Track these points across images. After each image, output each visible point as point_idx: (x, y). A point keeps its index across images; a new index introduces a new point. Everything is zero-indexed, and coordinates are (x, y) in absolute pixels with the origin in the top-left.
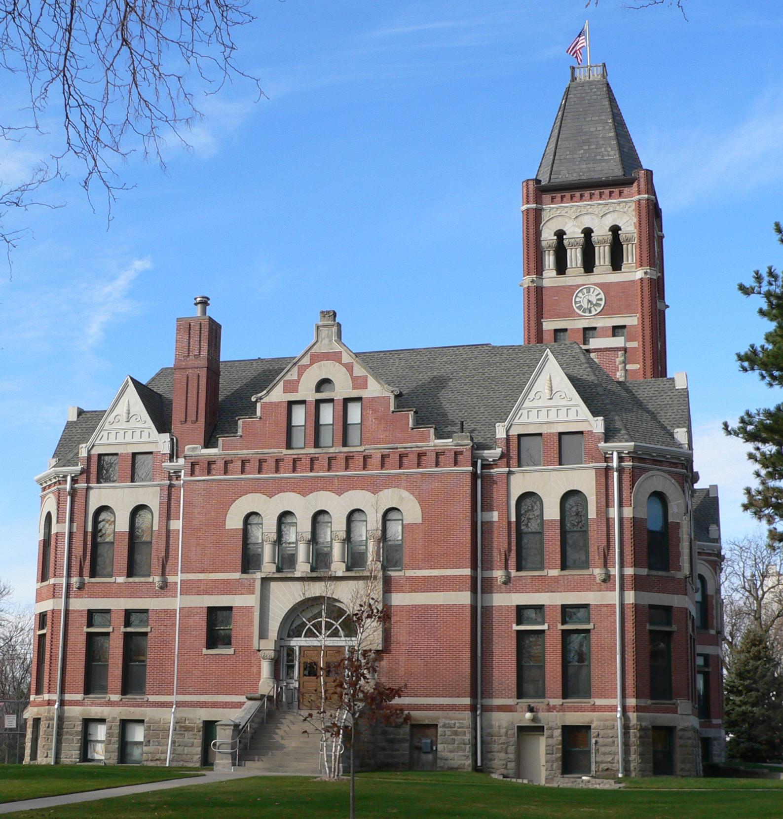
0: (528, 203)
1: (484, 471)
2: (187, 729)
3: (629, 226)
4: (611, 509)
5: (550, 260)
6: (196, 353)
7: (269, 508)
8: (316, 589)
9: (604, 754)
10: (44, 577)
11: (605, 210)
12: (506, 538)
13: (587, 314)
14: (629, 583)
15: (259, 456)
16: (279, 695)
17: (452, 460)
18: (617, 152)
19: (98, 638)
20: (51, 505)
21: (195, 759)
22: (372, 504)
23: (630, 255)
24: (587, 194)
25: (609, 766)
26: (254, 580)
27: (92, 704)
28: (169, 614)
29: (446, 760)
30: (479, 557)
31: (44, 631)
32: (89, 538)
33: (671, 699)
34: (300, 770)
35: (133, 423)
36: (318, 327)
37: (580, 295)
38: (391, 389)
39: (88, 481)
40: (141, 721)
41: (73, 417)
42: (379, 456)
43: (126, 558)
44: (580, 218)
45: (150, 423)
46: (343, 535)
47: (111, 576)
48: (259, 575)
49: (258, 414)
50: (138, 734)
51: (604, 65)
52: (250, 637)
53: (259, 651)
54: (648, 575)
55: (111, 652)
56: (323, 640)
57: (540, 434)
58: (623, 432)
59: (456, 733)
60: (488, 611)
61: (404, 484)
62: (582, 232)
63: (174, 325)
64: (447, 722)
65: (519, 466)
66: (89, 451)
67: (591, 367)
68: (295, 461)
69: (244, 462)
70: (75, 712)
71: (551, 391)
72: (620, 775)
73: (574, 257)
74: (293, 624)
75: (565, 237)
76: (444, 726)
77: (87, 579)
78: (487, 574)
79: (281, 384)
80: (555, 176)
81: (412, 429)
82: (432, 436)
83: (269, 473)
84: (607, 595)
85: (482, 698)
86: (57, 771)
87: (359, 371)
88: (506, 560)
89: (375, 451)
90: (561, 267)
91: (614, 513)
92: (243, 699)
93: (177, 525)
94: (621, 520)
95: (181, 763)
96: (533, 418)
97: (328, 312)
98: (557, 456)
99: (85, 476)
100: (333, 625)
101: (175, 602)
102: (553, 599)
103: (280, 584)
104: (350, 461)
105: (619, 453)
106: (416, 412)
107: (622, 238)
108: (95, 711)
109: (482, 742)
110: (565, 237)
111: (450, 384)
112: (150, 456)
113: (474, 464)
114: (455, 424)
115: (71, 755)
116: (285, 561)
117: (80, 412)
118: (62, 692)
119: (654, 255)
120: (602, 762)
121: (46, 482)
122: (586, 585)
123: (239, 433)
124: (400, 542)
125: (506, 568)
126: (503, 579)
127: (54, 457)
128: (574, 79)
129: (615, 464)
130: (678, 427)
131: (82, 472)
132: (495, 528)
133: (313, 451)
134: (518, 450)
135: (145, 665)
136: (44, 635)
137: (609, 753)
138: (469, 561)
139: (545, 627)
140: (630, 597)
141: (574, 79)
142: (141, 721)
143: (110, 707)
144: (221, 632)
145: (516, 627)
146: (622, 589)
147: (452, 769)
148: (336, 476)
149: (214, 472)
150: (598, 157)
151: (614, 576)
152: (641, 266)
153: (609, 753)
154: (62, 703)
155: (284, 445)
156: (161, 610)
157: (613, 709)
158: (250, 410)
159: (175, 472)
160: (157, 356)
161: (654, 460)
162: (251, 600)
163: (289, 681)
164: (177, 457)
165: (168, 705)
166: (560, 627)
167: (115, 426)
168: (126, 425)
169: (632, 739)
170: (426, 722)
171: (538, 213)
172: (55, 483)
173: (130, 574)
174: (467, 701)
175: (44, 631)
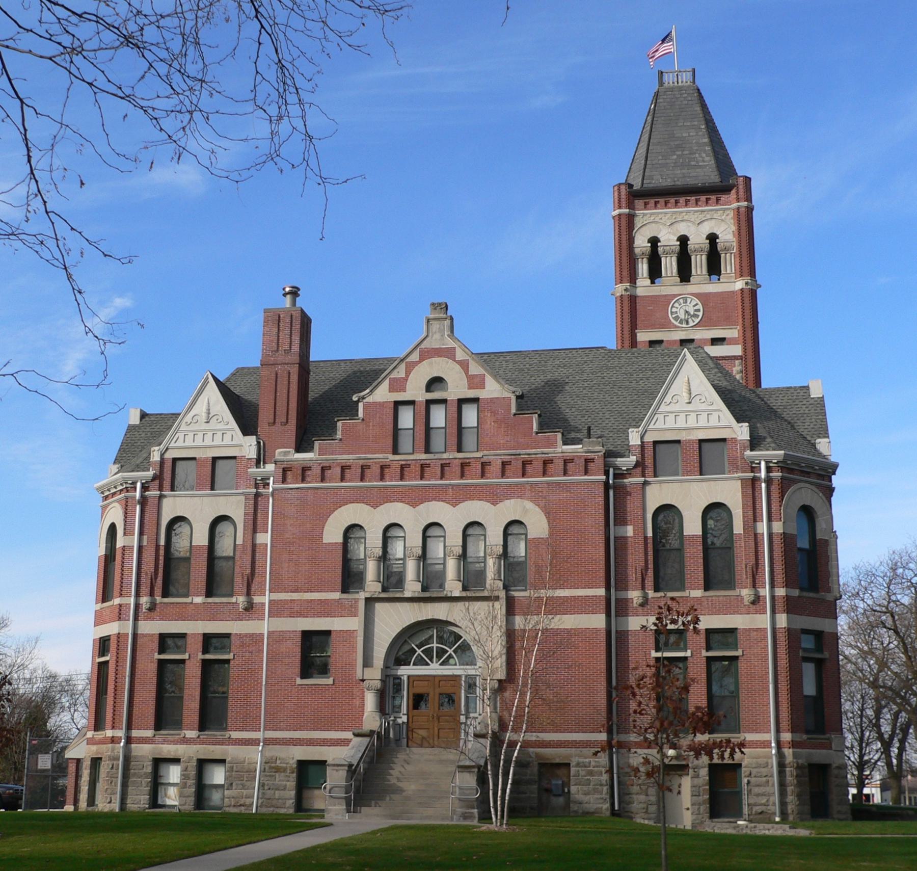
0: (620, 207)
1: (617, 481)
2: (278, 770)
3: (727, 234)
4: (759, 524)
5: (643, 268)
6: (287, 347)
7: (372, 520)
9: (758, 795)
10: (105, 595)
11: (702, 217)
12: (642, 555)
13: (684, 325)
14: (780, 605)
15: (361, 462)
16: (387, 731)
17: (582, 469)
18: (712, 158)
19: (216, 666)
20: (115, 514)
21: (287, 805)
22: (494, 516)
23: (729, 264)
24: (682, 200)
25: (763, 808)
26: (356, 600)
27: (165, 742)
28: (256, 639)
29: (580, 803)
30: (614, 576)
32: (162, 552)
33: (824, 734)
34: (427, 817)
35: (213, 425)
36: (428, 320)
37: (676, 305)
38: (511, 388)
39: (161, 488)
40: (222, 761)
41: (135, 419)
42: (499, 463)
43: (205, 576)
44: (675, 225)
45: (233, 424)
46: (459, 551)
47: (187, 596)
48: (362, 595)
49: (361, 414)
50: (218, 776)
51: (694, 71)
52: (353, 665)
53: (363, 680)
54: (799, 597)
55: (186, 681)
56: (434, 669)
57: (678, 442)
58: (769, 440)
59: (591, 773)
60: (623, 635)
61: (528, 494)
62: (678, 240)
63: (261, 316)
64: (581, 760)
65: (655, 476)
66: (162, 455)
67: (721, 373)
68: (402, 467)
69: (344, 468)
70: (144, 751)
71: (690, 394)
72: (777, 819)
73: (669, 265)
74: (400, 651)
76: (578, 765)
77: (158, 599)
78: (622, 595)
79: (387, 382)
80: (648, 181)
81: (537, 433)
82: (560, 442)
83: (376, 480)
84: (755, 617)
85: (618, 733)
86: (121, 822)
87: (475, 369)
88: (643, 580)
89: (495, 457)
90: (655, 273)
91: (762, 527)
92: (348, 735)
93: (265, 538)
94: (770, 535)
95: (271, 809)
96: (670, 423)
97: (440, 304)
98: (697, 465)
99: (157, 482)
100: (447, 651)
101: (264, 625)
103: (387, 605)
104: (466, 468)
105: (767, 462)
106: (540, 416)
107: (720, 247)
108: (168, 750)
109: (619, 783)
111: (567, 388)
112: (233, 461)
113: (607, 473)
114: (579, 431)
115: (139, 801)
116: (392, 581)
117: (143, 415)
118: (129, 727)
119: (749, 267)
120: (755, 805)
121: (109, 490)
122: (733, 607)
123: (339, 436)
124: (523, 559)
125: (643, 588)
126: (641, 600)
127: (115, 463)
128: (661, 83)
129: (763, 474)
130: (819, 437)
131: (154, 478)
132: (629, 543)
133: (424, 456)
134: (658, 456)
135: (227, 697)
136: (107, 662)
137: (763, 795)
138: (603, 579)
140: (782, 620)
141: (661, 83)
142: (222, 761)
143: (185, 745)
144: (318, 659)
145: (654, 654)
146: (773, 612)
147: (588, 813)
148: (450, 484)
149: (308, 479)
150: (693, 163)
151: (765, 597)
152: (742, 276)
153: (763, 795)
154: (129, 740)
155: (391, 450)
156: (246, 635)
157: (767, 744)
158: (351, 410)
159: (262, 479)
160: (244, 346)
161: (802, 472)
162: (354, 624)
163: (396, 715)
164: (264, 463)
165: (254, 742)
166: (705, 653)
167: (193, 427)
168: (205, 427)
169: (789, 779)
170: (557, 761)
171: (631, 219)
172: (122, 490)
173: (209, 593)
174: (603, 737)
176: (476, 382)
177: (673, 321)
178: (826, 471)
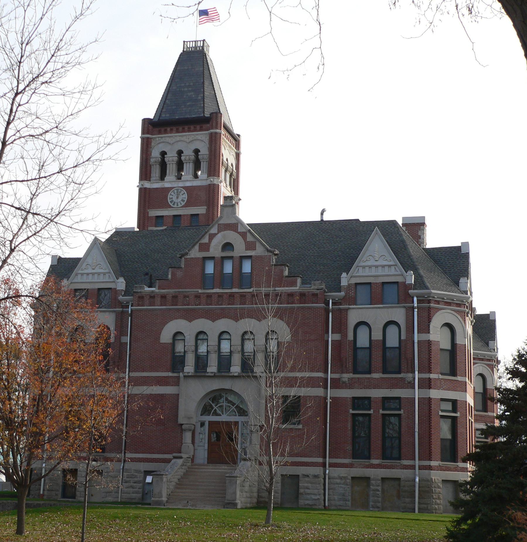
3: (204, 151)
8: (226, 384)
75: (199, 153)
79: (198, 244)
110: (199, 153)
116: (201, 363)
139: (371, 412)
154: (324, 465)
176: (250, 246)
177: (170, 203)
178: (463, 301)
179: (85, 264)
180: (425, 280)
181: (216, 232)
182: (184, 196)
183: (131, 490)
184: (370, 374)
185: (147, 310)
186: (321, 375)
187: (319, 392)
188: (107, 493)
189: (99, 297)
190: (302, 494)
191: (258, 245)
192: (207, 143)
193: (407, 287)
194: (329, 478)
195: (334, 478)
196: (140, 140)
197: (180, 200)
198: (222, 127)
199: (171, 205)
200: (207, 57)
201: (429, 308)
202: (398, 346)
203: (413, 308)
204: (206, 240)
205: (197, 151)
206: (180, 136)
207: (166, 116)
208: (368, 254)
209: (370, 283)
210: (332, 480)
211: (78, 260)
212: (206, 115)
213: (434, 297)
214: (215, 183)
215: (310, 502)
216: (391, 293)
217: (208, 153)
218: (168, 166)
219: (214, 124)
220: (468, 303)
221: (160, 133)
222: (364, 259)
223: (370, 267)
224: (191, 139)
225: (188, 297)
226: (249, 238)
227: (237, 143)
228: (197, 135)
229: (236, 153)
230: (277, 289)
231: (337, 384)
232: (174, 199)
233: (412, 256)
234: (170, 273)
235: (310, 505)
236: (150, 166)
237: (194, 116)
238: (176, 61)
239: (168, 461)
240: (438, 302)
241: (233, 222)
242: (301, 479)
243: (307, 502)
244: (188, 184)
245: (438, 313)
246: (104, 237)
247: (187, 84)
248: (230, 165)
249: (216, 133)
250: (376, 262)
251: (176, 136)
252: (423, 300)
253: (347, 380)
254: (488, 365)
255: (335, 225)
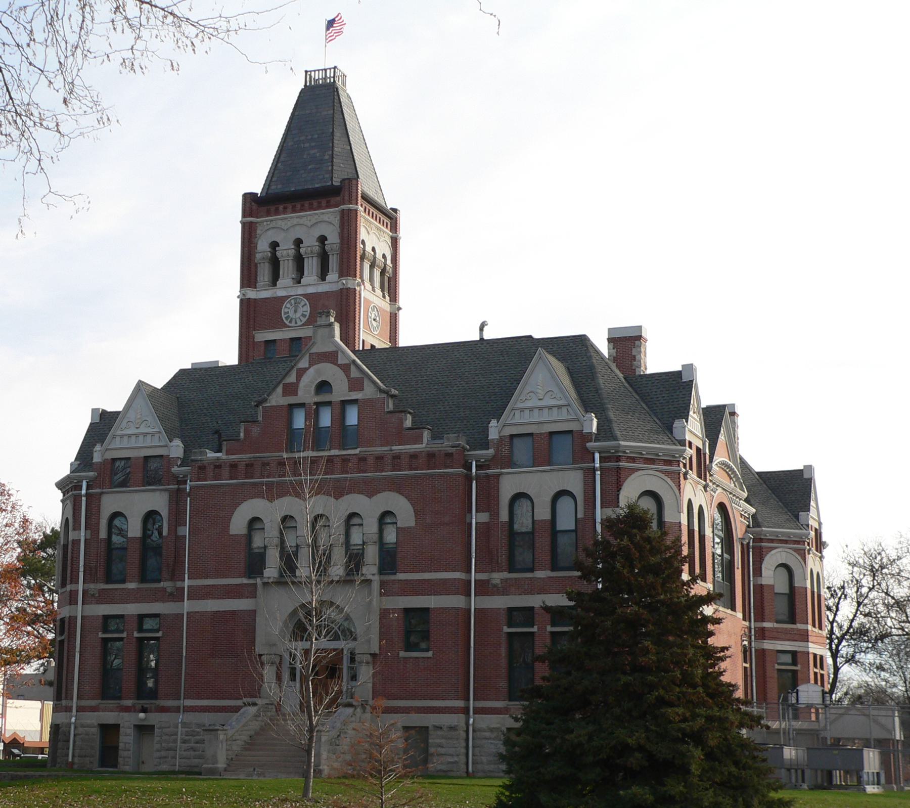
3: (333, 239)
22: (369, 507)
31: (63, 638)
79: (281, 385)
93: (185, 531)
96: (527, 417)
102: (131, 609)
139: (535, 629)
154: (466, 711)
175: (63, 638)
176: (356, 384)
178: (674, 456)
179: (125, 421)
180: (615, 426)
181: (307, 366)
182: (305, 309)
183: (192, 753)
184: (532, 571)
185: (211, 485)
186: (457, 575)
187: (455, 601)
188: (160, 758)
189: (149, 471)
190: (432, 755)
191: (366, 382)
192: (337, 226)
193: (586, 437)
194: (474, 731)
195: (480, 730)
196: (240, 225)
197: (298, 315)
198: (360, 198)
199: (287, 322)
200: (341, 92)
201: (618, 469)
202: (573, 528)
203: (594, 470)
204: (292, 378)
205: (322, 239)
206: (298, 217)
207: (277, 188)
208: (528, 389)
209: (531, 435)
210: (478, 733)
211: (118, 413)
212: (335, 184)
213: (624, 452)
214: (349, 286)
215: (444, 767)
216: (564, 448)
217: (338, 241)
218: (281, 263)
219: (347, 197)
220: (684, 458)
221: (268, 214)
222: (523, 398)
223: (531, 409)
224: (314, 221)
225: (268, 464)
226: (354, 373)
227: (393, 221)
228: (323, 214)
229: (392, 237)
230: (394, 448)
231: (484, 588)
232: (291, 314)
233: (601, 389)
234: (242, 430)
235: (444, 771)
236: (256, 265)
237: (317, 186)
238: (295, 102)
239: (236, 709)
240: (633, 460)
241: (330, 350)
242: (431, 732)
243: (439, 767)
244: (311, 290)
245: (633, 476)
246: (159, 380)
247: (310, 137)
248: (379, 256)
249: (350, 210)
250: (543, 401)
251: (291, 218)
252: (608, 457)
253: (498, 581)
254: (796, 550)
255: (495, 346)
